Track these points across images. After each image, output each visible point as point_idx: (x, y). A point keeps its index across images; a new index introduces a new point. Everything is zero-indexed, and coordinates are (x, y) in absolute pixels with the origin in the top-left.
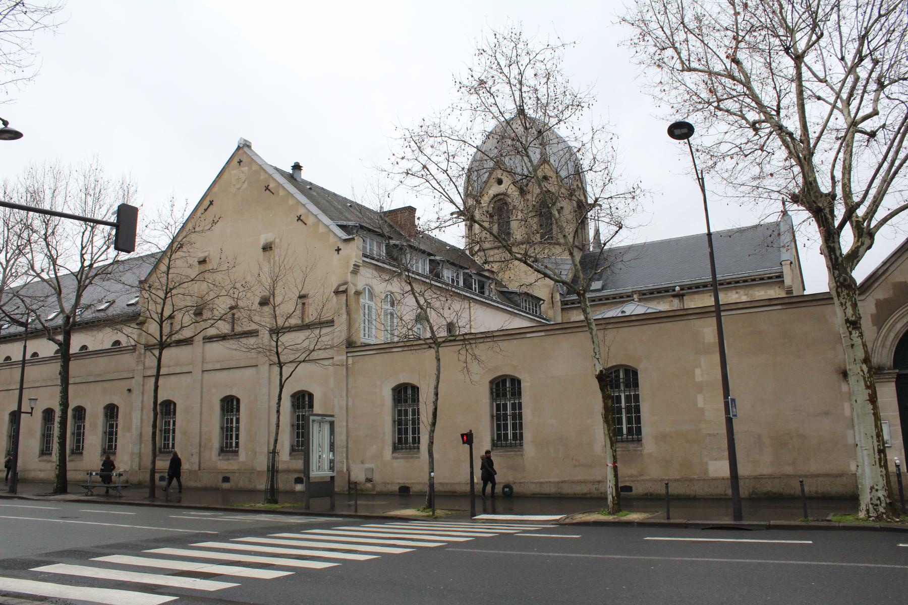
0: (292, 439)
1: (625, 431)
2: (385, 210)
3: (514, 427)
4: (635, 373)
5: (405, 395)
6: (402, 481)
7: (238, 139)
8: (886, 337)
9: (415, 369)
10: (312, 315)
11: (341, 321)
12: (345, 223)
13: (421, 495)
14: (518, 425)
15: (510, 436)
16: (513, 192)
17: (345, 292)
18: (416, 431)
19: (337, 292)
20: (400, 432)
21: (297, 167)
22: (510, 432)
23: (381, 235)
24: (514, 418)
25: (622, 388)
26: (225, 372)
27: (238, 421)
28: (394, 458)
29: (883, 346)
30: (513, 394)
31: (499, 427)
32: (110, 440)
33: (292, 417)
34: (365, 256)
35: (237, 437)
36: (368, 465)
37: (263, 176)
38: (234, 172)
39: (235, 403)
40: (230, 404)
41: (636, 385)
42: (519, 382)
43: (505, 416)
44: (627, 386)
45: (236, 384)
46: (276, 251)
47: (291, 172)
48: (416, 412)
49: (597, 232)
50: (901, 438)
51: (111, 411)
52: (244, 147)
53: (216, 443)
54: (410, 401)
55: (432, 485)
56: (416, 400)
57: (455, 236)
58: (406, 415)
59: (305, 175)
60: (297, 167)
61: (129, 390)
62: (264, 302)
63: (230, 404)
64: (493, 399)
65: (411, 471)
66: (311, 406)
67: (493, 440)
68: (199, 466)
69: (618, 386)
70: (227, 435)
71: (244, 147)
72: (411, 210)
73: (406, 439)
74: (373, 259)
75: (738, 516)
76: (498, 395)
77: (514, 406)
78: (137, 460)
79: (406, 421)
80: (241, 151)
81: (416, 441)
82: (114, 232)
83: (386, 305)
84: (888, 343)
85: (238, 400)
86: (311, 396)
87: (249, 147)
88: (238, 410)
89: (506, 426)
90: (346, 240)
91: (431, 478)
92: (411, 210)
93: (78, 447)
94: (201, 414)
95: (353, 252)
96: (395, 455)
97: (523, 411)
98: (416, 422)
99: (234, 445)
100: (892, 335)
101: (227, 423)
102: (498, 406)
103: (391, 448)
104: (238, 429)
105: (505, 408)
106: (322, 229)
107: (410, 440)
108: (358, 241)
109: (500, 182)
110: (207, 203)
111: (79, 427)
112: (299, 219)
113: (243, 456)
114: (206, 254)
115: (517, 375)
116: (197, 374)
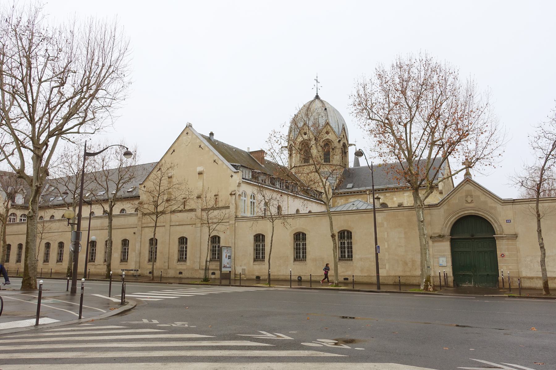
0: (178, 256)
2: (250, 151)
3: (303, 253)
5: (259, 238)
6: (257, 274)
8: (447, 223)
9: (264, 227)
10: (220, 204)
11: (232, 207)
12: (235, 164)
13: (265, 280)
14: (304, 253)
15: (301, 257)
17: (235, 194)
18: (263, 253)
19: (231, 194)
20: (297, 253)
21: (212, 134)
22: (301, 255)
23: (250, 169)
24: (303, 250)
26: (181, 226)
27: (186, 248)
30: (303, 240)
32: (60, 256)
34: (243, 179)
35: (186, 255)
38: (184, 137)
40: (183, 241)
41: (351, 238)
43: (300, 248)
44: (348, 238)
45: (185, 231)
46: (205, 175)
48: (264, 246)
51: (125, 243)
52: (189, 126)
53: (176, 256)
54: (261, 241)
55: (269, 275)
56: (263, 240)
57: (283, 160)
58: (259, 247)
59: (215, 137)
60: (212, 134)
61: (134, 233)
62: (199, 197)
63: (183, 241)
64: (179, 245)
65: (261, 269)
66: (219, 242)
69: (344, 238)
71: (189, 126)
74: (246, 179)
75: (379, 288)
76: (297, 240)
77: (303, 244)
78: (138, 265)
79: (259, 249)
80: (187, 129)
81: (263, 258)
82: (4, 82)
83: (249, 197)
84: (448, 226)
85: (186, 239)
86: (219, 238)
87: (191, 126)
88: (186, 243)
89: (300, 252)
91: (269, 271)
93: (60, 259)
95: (237, 178)
98: (263, 250)
100: (449, 223)
102: (297, 244)
104: (186, 251)
106: (225, 167)
107: (261, 257)
108: (240, 173)
110: (171, 151)
111: (93, 250)
112: (215, 161)
115: (304, 232)
116: (168, 226)
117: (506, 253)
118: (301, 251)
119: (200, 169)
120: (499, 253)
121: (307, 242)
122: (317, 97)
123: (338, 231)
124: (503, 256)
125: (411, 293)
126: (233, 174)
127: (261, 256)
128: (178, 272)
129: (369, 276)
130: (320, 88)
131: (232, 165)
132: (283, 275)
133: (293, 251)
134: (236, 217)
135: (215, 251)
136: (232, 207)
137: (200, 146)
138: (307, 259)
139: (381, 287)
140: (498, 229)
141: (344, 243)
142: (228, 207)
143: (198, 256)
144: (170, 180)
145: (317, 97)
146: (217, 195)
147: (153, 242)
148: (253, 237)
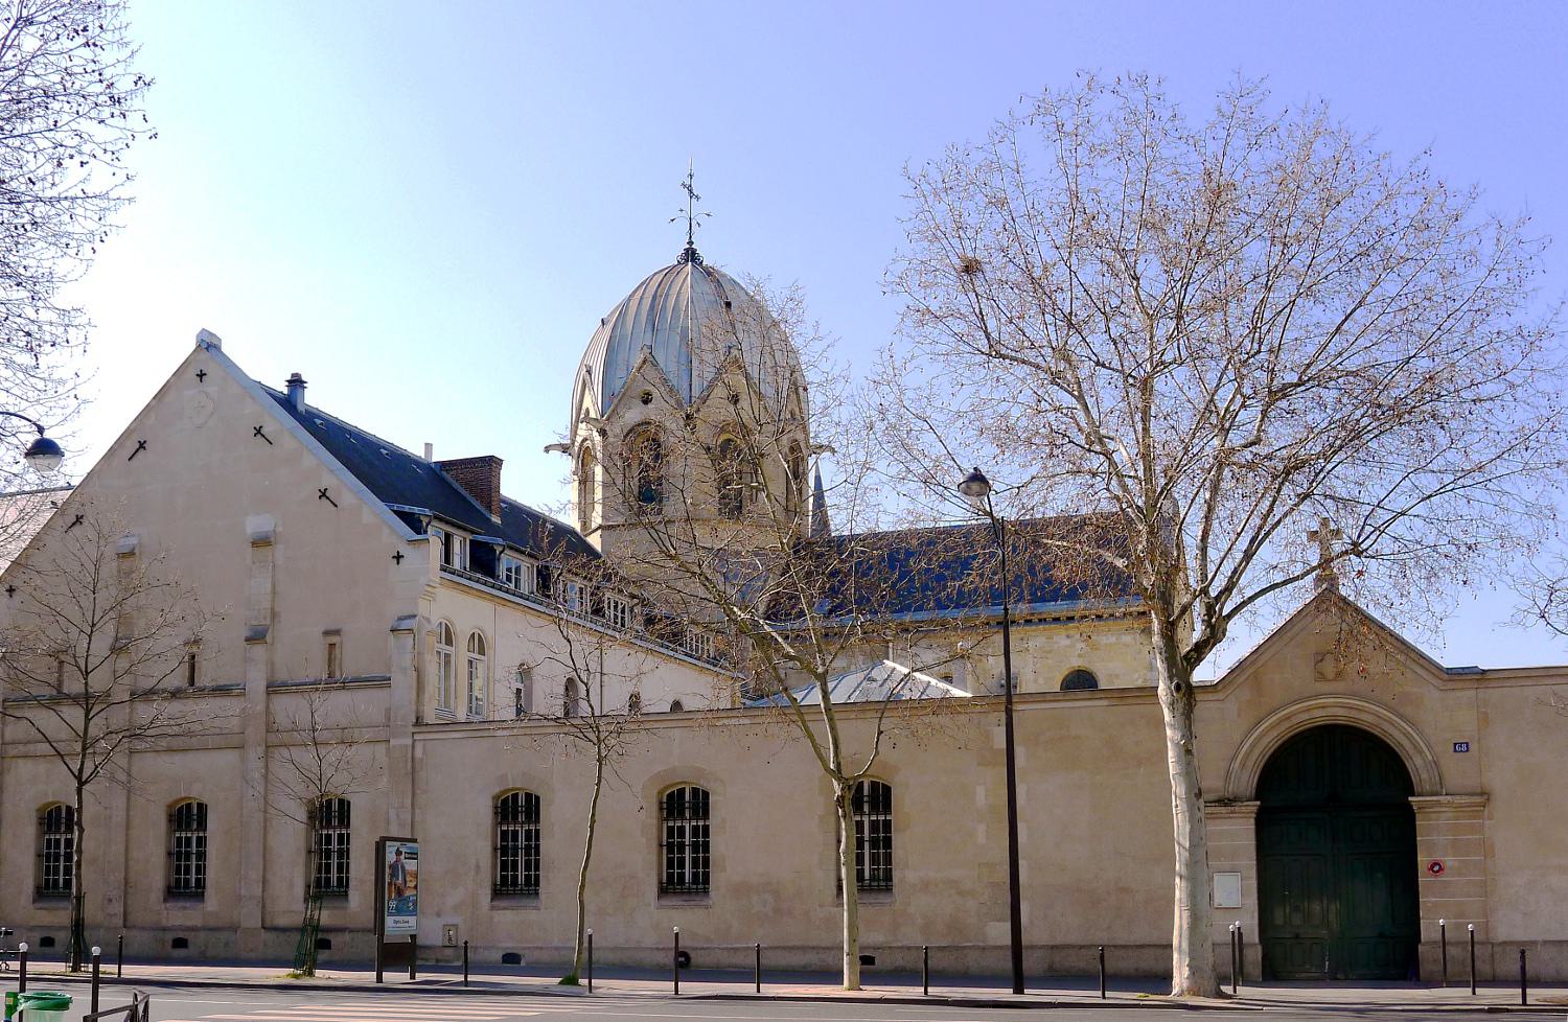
11: (403, 683)
12: (407, 508)
16: (673, 424)
21: (296, 382)
27: (201, 842)
28: (493, 908)
29: (1243, 766)
31: (670, 864)
33: (169, 841)
36: (450, 920)
40: (187, 818)
44: (529, 819)
46: (279, 552)
47: (286, 391)
49: (818, 479)
50: (1256, 895)
52: (208, 345)
58: (515, 839)
60: (296, 382)
63: (187, 818)
64: (41, 834)
67: (660, 883)
68: (125, 920)
70: (48, 867)
71: (208, 345)
72: (489, 466)
73: (515, 877)
75: (590, 991)
81: (344, 883)
84: (1250, 764)
92: (489, 466)
94: (128, 827)
96: (495, 903)
97: (712, 839)
101: (49, 847)
102: (670, 830)
103: (489, 891)
104: (202, 856)
105: (188, 844)
107: (521, 879)
109: (646, 399)
112: (323, 494)
113: (212, 901)
114: (133, 541)
117: (1449, 861)
118: (521, 859)
119: (255, 524)
120: (1423, 860)
121: (713, 822)
122: (691, 255)
123: (37, 807)
124: (1436, 868)
128: (170, 937)
129: (957, 948)
130: (702, 219)
131: (397, 513)
132: (615, 949)
133: (654, 858)
134: (418, 722)
136: (403, 683)
137: (258, 431)
138: (712, 886)
139: (28, 985)
140: (1424, 776)
141: (682, 830)
142: (383, 682)
143: (255, 875)
144: (126, 564)
145: (691, 255)
146: (337, 632)
147: (57, 821)
148: (490, 803)
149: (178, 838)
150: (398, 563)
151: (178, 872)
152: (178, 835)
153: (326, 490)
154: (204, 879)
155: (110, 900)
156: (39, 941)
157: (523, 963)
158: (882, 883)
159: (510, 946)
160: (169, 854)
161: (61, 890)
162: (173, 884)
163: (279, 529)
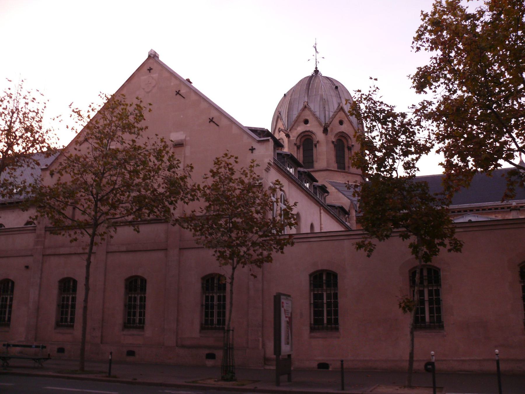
1: (325, 321)
4: (335, 276)
7: (149, 50)
20: (207, 315)
25: (325, 288)
27: (11, 300)
28: (311, 337)
37: (174, 82)
38: (144, 77)
39: (10, 285)
40: (135, 285)
41: (336, 285)
42: (146, 280)
44: (328, 286)
52: (153, 57)
53: (119, 318)
56: (143, 289)
58: (68, 301)
61: (27, 267)
67: (202, 324)
71: (153, 57)
79: (67, 305)
81: (72, 320)
85: (13, 283)
90: (259, 141)
96: (312, 334)
99: (69, 319)
102: (207, 297)
103: (308, 328)
104: (143, 307)
107: (137, 321)
109: (306, 122)
113: (148, 332)
123: (59, 280)
125: (150, 384)
126: (255, 145)
127: (137, 318)
135: (212, 307)
148: (308, 278)
149: (129, 297)
150: (252, 152)
151: (62, 314)
152: (63, 296)
153: (213, 118)
154: (144, 319)
155: (94, 329)
156: (56, 350)
157: (330, 369)
158: (436, 324)
159: (321, 359)
160: (125, 306)
161: (69, 323)
162: (204, 323)
163: (188, 138)
